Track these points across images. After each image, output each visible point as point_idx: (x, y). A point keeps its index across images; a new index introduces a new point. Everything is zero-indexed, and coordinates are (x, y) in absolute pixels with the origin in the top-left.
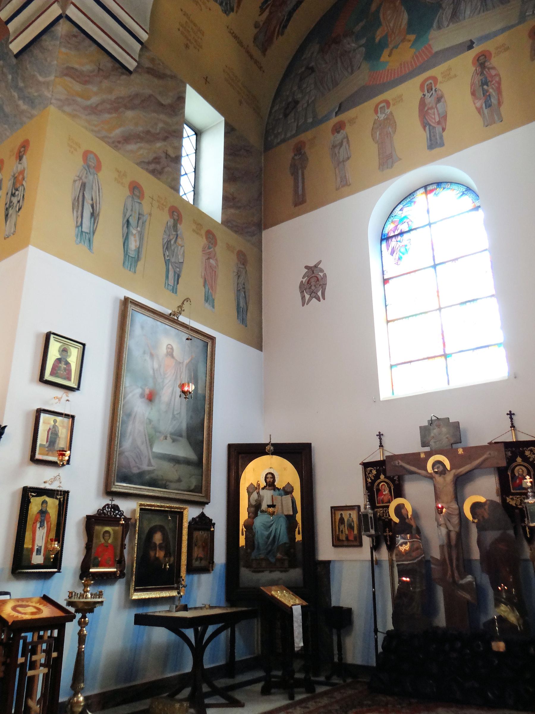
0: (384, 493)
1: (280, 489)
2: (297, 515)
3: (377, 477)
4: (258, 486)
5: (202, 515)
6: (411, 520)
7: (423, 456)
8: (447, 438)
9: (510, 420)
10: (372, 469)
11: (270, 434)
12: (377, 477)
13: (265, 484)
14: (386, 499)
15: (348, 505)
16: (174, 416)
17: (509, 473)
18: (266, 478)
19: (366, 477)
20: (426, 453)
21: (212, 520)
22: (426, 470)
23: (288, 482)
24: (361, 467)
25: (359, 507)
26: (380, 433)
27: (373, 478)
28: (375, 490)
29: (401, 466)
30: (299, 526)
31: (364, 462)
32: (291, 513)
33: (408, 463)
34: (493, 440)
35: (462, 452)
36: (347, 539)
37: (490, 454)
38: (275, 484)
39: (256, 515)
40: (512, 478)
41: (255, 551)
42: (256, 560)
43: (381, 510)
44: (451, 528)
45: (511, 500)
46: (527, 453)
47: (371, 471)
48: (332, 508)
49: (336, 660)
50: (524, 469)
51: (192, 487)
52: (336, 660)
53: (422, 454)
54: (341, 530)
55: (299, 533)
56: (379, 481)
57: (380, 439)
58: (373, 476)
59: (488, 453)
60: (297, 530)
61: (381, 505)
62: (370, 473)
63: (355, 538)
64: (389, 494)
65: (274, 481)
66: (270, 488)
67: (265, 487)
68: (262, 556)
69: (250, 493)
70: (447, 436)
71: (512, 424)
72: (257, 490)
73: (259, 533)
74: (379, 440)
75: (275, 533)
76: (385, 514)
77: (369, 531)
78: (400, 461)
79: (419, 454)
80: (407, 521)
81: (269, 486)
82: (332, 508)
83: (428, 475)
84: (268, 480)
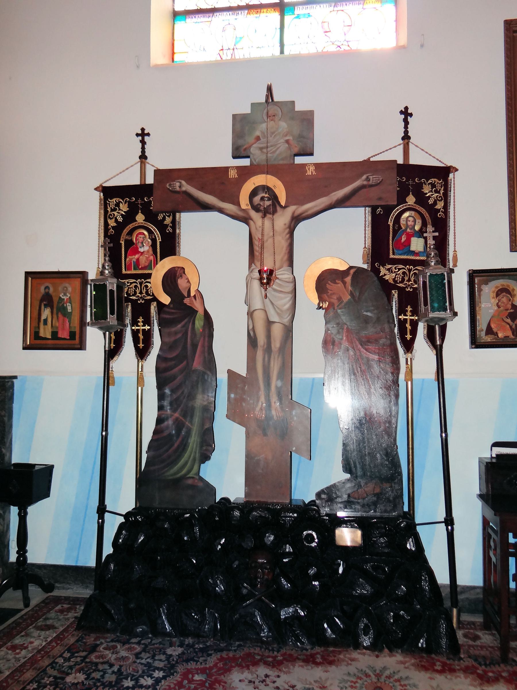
0: (141, 250)
3: (129, 217)
6: (195, 299)
7: (233, 174)
8: (287, 142)
9: (403, 124)
10: (122, 203)
11: (239, 682)
12: (129, 217)
14: (143, 261)
15: (61, 270)
17: (391, 223)
20: (240, 169)
22: (238, 204)
24: (97, 196)
25: (83, 274)
26: (143, 130)
27: (120, 219)
29: (186, 193)
31: (104, 185)
33: (202, 189)
34: (372, 157)
35: (314, 173)
36: (55, 335)
37: (368, 179)
40: (395, 233)
43: (131, 283)
44: (274, 317)
45: (387, 272)
46: (426, 189)
47: (118, 205)
49: (13, 557)
50: (417, 216)
52: (13, 557)
53: (232, 172)
54: (43, 317)
56: (131, 226)
57: (143, 142)
58: (122, 215)
59: (364, 177)
61: (133, 272)
62: (115, 210)
63: (72, 335)
64: (151, 252)
70: (287, 138)
71: (406, 132)
74: (141, 144)
76: (138, 291)
77: (105, 318)
78: (183, 182)
79: (226, 169)
80: (186, 301)
83: (241, 214)
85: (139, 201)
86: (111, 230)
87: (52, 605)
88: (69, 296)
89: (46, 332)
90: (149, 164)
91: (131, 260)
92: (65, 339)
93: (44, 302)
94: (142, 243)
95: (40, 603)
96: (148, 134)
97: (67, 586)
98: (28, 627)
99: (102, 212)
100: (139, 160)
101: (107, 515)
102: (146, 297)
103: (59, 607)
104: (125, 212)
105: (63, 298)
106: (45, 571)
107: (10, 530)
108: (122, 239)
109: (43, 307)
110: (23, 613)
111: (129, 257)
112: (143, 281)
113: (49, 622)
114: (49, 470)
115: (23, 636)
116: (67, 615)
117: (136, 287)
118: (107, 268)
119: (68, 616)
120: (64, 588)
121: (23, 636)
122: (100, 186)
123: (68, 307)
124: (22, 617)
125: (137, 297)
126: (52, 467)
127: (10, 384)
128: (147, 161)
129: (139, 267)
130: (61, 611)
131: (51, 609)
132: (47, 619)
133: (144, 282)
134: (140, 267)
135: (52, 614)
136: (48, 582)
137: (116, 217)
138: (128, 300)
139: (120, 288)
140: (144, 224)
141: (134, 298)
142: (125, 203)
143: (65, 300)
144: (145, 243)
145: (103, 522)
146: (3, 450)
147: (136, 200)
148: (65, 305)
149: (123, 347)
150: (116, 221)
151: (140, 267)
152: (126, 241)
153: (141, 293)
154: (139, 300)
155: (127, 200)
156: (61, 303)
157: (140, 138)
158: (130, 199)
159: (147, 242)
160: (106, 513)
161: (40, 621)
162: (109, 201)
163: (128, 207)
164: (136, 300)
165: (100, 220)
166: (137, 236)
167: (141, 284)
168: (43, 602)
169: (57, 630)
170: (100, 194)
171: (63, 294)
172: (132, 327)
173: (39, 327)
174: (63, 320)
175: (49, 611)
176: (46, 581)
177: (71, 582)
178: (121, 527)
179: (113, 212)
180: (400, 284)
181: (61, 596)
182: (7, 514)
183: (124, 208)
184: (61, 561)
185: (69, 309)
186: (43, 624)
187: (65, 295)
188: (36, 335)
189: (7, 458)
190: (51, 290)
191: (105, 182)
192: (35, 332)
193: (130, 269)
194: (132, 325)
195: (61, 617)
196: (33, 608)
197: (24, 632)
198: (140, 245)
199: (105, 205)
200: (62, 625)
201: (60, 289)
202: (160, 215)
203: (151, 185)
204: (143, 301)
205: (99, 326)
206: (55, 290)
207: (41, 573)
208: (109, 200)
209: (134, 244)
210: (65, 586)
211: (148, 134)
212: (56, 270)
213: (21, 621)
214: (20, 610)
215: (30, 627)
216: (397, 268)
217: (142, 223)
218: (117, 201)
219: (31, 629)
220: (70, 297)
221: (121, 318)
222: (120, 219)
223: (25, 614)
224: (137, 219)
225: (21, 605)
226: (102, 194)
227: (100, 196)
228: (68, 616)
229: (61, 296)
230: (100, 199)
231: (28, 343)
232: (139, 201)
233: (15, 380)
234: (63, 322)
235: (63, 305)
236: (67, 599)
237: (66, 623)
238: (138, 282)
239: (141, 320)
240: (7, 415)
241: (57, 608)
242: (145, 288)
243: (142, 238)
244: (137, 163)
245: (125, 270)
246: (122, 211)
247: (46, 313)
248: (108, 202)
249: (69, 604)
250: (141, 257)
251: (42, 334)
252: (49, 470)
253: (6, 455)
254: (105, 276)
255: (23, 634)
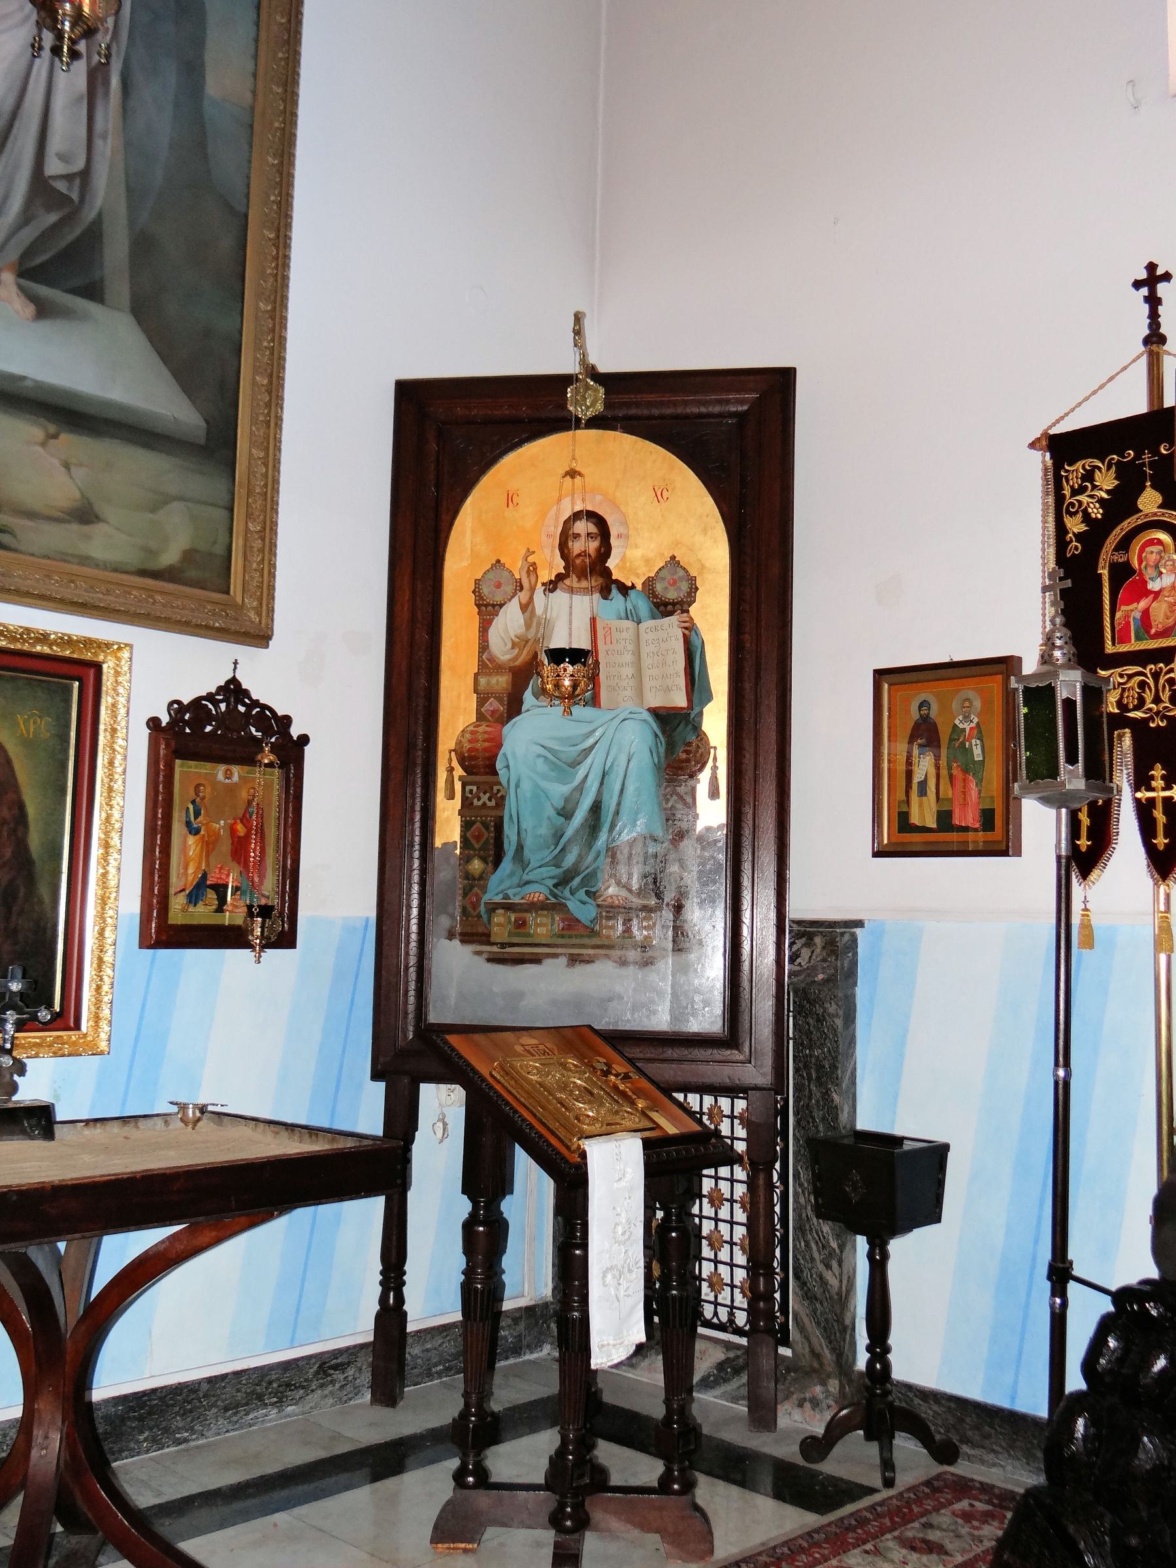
0: (1153, 586)
1: (633, 587)
2: (708, 710)
4: (528, 572)
5: (233, 690)
10: (1099, 469)
13: (559, 566)
16: (39, 182)
18: (565, 537)
19: (1060, 508)
21: (287, 721)
23: (673, 558)
24: (1039, 461)
25: (1007, 665)
26: (1151, 267)
27: (1096, 512)
28: (1104, 572)
30: (715, 759)
31: (1052, 432)
32: (681, 701)
36: (945, 820)
38: (611, 563)
39: (514, 707)
41: (507, 865)
42: (509, 907)
43: (1130, 677)
47: (1089, 476)
48: (876, 672)
49: (862, 1360)
51: (170, 557)
54: (917, 777)
55: (714, 794)
57: (1153, 301)
58: (1101, 501)
60: (704, 777)
61: (1134, 646)
62: (1082, 490)
65: (605, 550)
66: (584, 584)
67: (560, 577)
68: (538, 893)
69: (487, 610)
72: (523, 596)
73: (526, 786)
74: (1146, 307)
75: (600, 792)
76: (1149, 696)
77: (1054, 773)
81: (582, 575)
82: (876, 672)
84: (577, 547)
85: (1147, 457)
86: (1074, 543)
87: (949, 1497)
88: (976, 720)
89: (924, 813)
90: (1169, 354)
91: (1127, 616)
92: (966, 829)
93: (919, 741)
94: (1157, 566)
95: (920, 1484)
96: (1167, 277)
97: (991, 1457)
98: (882, 1535)
99: (1051, 500)
100: (1143, 348)
101: (1072, 1287)
102: (1171, 710)
103: (964, 1504)
104: (1108, 492)
105: (961, 726)
106: (935, 1408)
107: (855, 1294)
108: (1101, 563)
109: (916, 752)
110: (877, 1497)
111: (1124, 608)
112: (1161, 669)
113: (934, 1536)
114: (937, 1154)
115: (867, 1552)
116: (977, 1528)
117: (1142, 685)
118: (1058, 643)
119: (981, 1533)
120: (982, 1462)
121: (867, 1552)
122: (1042, 435)
123: (974, 747)
124: (872, 1508)
125: (1146, 713)
126: (945, 1148)
127: (847, 937)
128: (1165, 348)
129: (1148, 632)
130: (967, 1517)
131: (943, 1506)
132: (928, 1526)
133: (1165, 670)
134: (1153, 631)
135: (944, 1518)
136: (944, 1437)
137: (1086, 508)
138: (1118, 721)
139: (1093, 695)
140: (1160, 516)
141: (1138, 714)
142: (1109, 469)
143: (967, 731)
144: (1165, 566)
145: (1064, 1304)
146: (834, 1095)
147: (1138, 456)
148: (967, 744)
149: (1113, 846)
150: (1087, 517)
151: (1153, 631)
152: (1114, 568)
153: (1157, 700)
154: (1152, 719)
155: (1113, 459)
156: (959, 739)
157: (1145, 291)
158: (1122, 455)
159: (1170, 563)
160: (1071, 1282)
161: (912, 1528)
162: (1067, 471)
163: (1115, 478)
164: (1145, 721)
165: (1044, 522)
166: (1142, 550)
167: (1156, 676)
168: (928, 1483)
169: (949, 1558)
170: (1044, 457)
171: (961, 718)
172: (1136, 791)
173: (908, 802)
174: (964, 780)
175: (937, 1510)
176: (940, 1433)
177: (1001, 1450)
178: (1106, 1326)
179: (1077, 498)
180: (1136, 712)
181: (972, 1480)
182: (848, 1247)
183: (1106, 481)
184: (974, 1392)
185: (977, 752)
186: (921, 1535)
187: (967, 718)
188: (903, 823)
189: (844, 1117)
190: (934, 713)
191: (1054, 424)
192: (900, 813)
193: (1125, 639)
194: (1137, 788)
195: (964, 1530)
196: (901, 1494)
197: (873, 1543)
198: (1149, 573)
199: (1055, 480)
200: (963, 1552)
201: (955, 705)
202: (1098, 512)
203: (1172, 408)
204: (1162, 721)
205: (1039, 795)
206: (945, 707)
207: (926, 1411)
208: (1067, 467)
209: (1133, 572)
210: (985, 1457)
211: (1167, 277)
212: (945, 659)
213: (869, 1515)
214: (872, 1491)
215: (888, 1536)
216: (1126, 674)
217: (1155, 514)
218: (1088, 468)
219: (888, 1541)
220: (978, 724)
221: (1098, 771)
222: (1096, 512)
223: (882, 1503)
224: (1140, 507)
225: (876, 1481)
226: (1048, 455)
227: (1044, 462)
228: (981, 1533)
229: (957, 722)
230: (1046, 470)
231: (886, 842)
232: (1147, 457)
233: (858, 931)
234: (964, 787)
235: (963, 743)
236: (986, 1489)
237: (974, 1547)
238: (1147, 671)
239: (1158, 772)
240: (841, 1013)
241: (958, 1506)
242: (1167, 688)
243: (1154, 555)
244: (1142, 354)
245: (1114, 644)
246: (1101, 489)
247: (924, 766)
248: (1063, 474)
249: (989, 1502)
250: (1155, 604)
251: (915, 819)
252: (937, 1154)
253: (842, 1111)
254: (1054, 665)
255: (869, 1547)
